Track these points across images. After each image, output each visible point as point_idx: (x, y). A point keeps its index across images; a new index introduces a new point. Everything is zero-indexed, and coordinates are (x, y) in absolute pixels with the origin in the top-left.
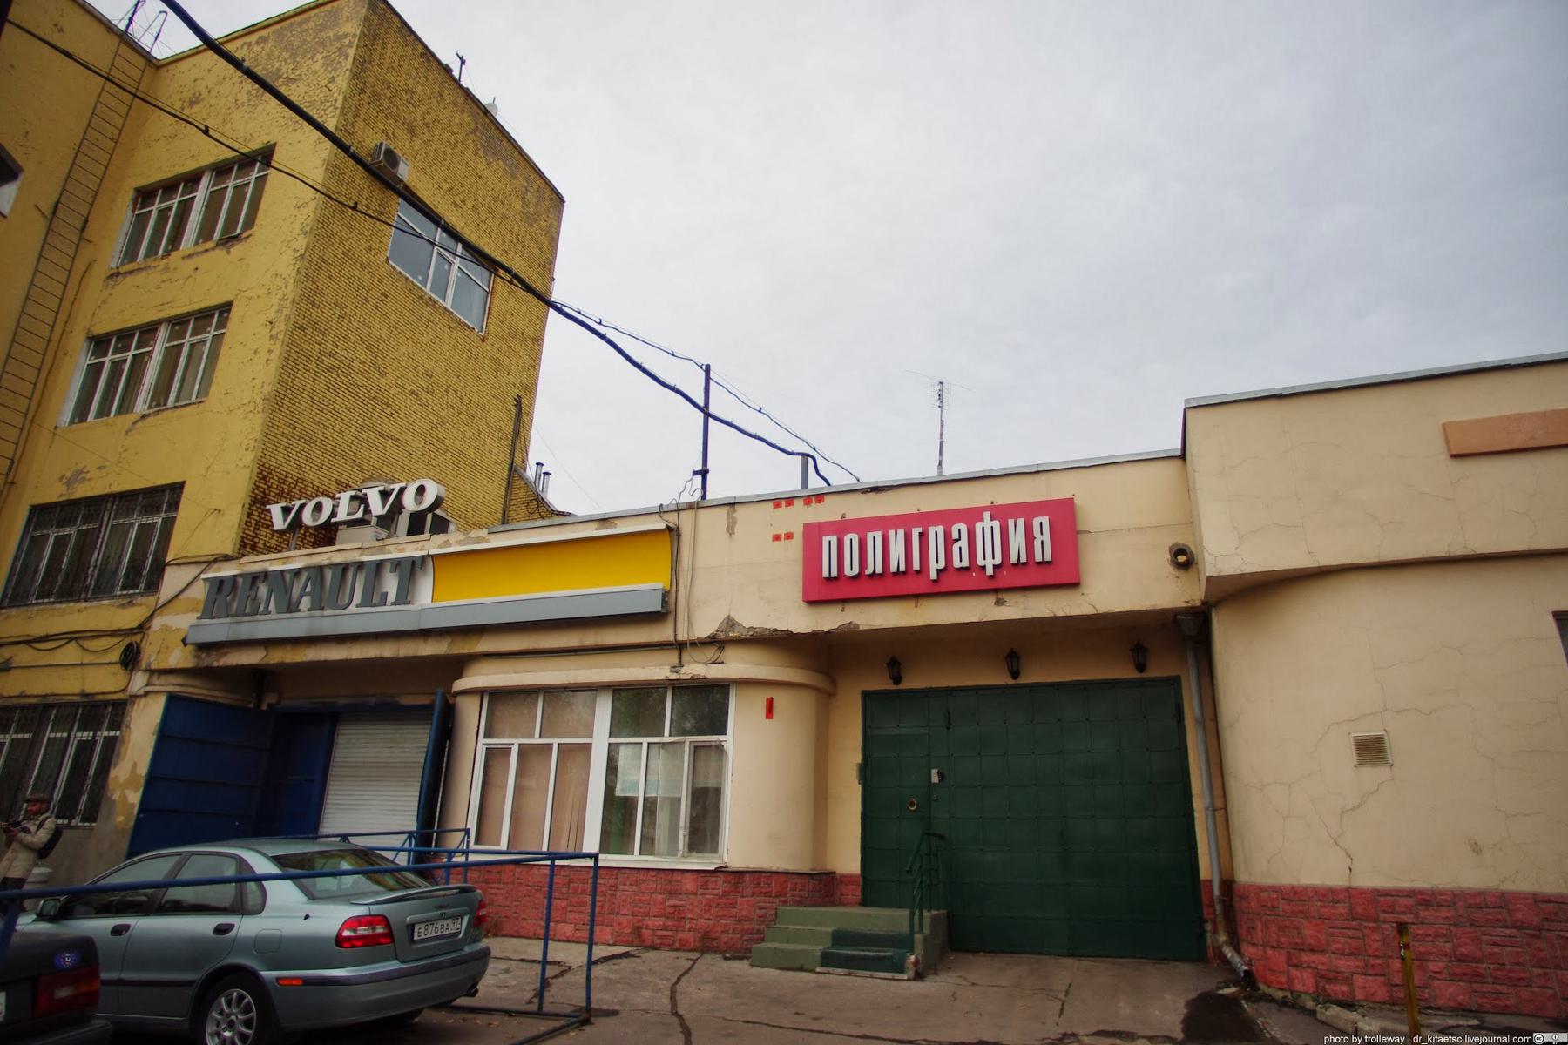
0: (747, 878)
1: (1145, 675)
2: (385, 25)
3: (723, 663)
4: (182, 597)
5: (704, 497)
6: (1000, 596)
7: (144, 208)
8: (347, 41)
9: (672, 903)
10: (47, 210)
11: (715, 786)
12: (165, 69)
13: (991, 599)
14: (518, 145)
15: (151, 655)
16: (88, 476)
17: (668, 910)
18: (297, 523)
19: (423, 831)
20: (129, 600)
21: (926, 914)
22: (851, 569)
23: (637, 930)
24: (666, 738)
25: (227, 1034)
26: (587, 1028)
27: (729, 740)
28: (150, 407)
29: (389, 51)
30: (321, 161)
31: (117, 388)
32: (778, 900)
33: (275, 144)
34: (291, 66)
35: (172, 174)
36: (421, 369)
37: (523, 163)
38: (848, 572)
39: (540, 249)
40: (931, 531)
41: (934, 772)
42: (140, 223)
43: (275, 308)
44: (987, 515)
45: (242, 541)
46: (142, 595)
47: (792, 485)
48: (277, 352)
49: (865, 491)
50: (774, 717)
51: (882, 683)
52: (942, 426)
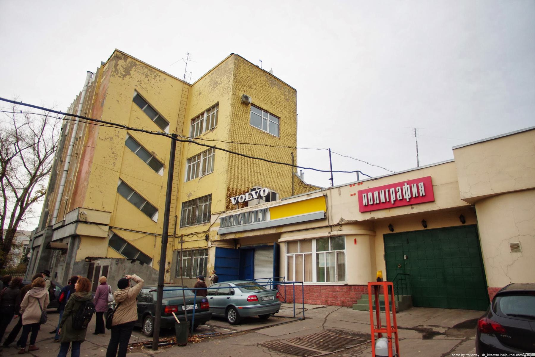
0: (352, 287)
1: (465, 224)
2: (240, 62)
3: (342, 230)
5: (333, 185)
6: (412, 206)
8: (231, 70)
9: (334, 294)
11: (343, 263)
12: (193, 86)
13: (410, 207)
14: (280, 79)
15: (211, 238)
17: (333, 296)
18: (237, 202)
19: (275, 278)
20: (204, 224)
21: (400, 296)
22: (371, 203)
23: (326, 301)
24: (330, 251)
25: (231, 317)
26: (303, 321)
27: (345, 251)
28: (202, 175)
29: (242, 68)
30: (230, 104)
31: (194, 174)
32: (361, 293)
33: (219, 102)
34: (220, 80)
36: (263, 152)
37: (283, 84)
38: (370, 203)
39: (292, 108)
40: (391, 190)
41: (405, 256)
42: (193, 127)
43: (225, 146)
44: (406, 184)
45: (226, 207)
46: (207, 222)
47: (355, 180)
48: (227, 157)
49: (373, 180)
50: (357, 243)
51: (388, 232)
52: (417, 143)
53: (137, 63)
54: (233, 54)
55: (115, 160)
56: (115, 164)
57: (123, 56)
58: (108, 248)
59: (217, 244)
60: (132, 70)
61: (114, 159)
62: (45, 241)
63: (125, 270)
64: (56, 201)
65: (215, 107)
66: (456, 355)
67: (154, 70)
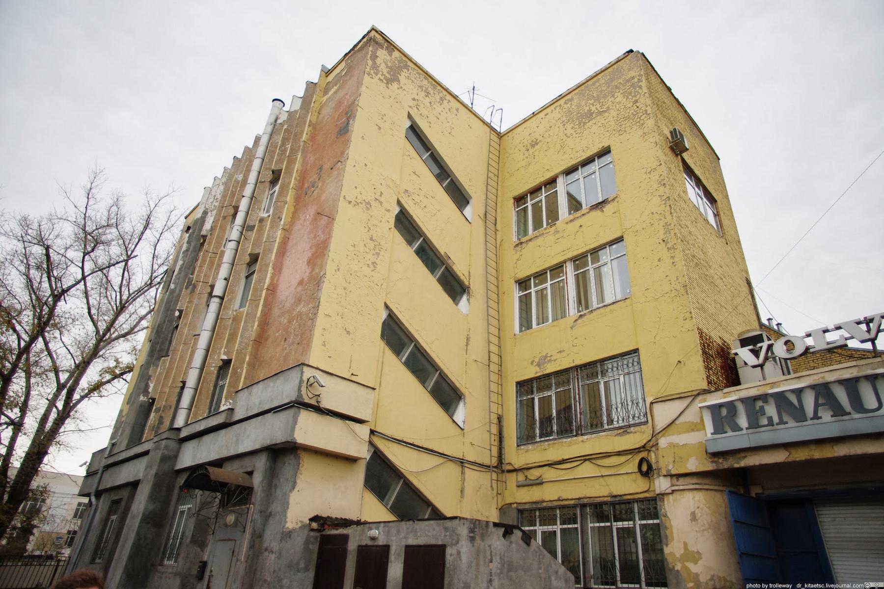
4: (677, 422)
10: (482, 216)
35: (538, 183)
53: (409, 63)
54: (631, 51)
55: (376, 256)
56: (376, 266)
59: (693, 484)
60: (403, 74)
61: (373, 254)
62: (158, 469)
63: (491, 562)
64: (189, 367)
65: (541, 188)
66: (753, 586)
67: (439, 88)
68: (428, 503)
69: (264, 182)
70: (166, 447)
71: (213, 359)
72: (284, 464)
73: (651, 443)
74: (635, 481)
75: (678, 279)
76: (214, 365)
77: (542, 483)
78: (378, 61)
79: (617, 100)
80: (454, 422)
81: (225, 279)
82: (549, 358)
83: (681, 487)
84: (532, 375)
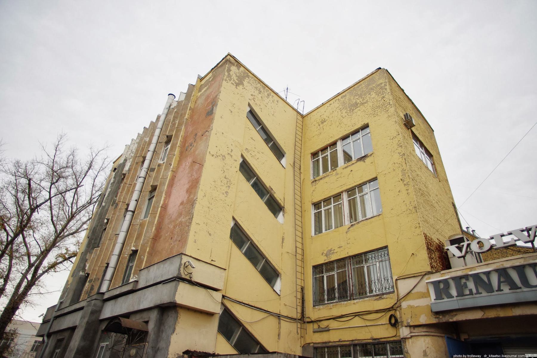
4: (413, 292)
7: (314, 159)
10: (292, 164)
16: (335, 251)
53: (250, 74)
54: (380, 68)
57: (235, 62)
58: (217, 334)
59: (424, 332)
61: (226, 187)
62: (89, 319)
65: (327, 148)
66: (457, 356)
67: (267, 88)
68: (258, 343)
69: (162, 142)
70: (95, 305)
71: (127, 249)
72: (168, 316)
73: (397, 305)
74: (387, 329)
75: (410, 203)
76: (127, 253)
77: (329, 330)
78: (231, 73)
79: (372, 96)
80: (274, 290)
81: (136, 200)
82: (333, 251)
83: (416, 334)
84: (322, 262)
